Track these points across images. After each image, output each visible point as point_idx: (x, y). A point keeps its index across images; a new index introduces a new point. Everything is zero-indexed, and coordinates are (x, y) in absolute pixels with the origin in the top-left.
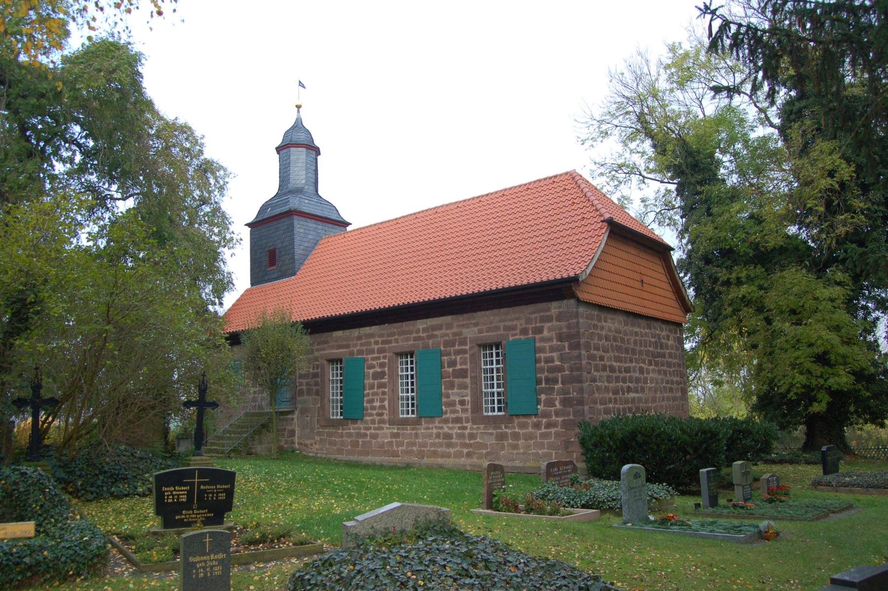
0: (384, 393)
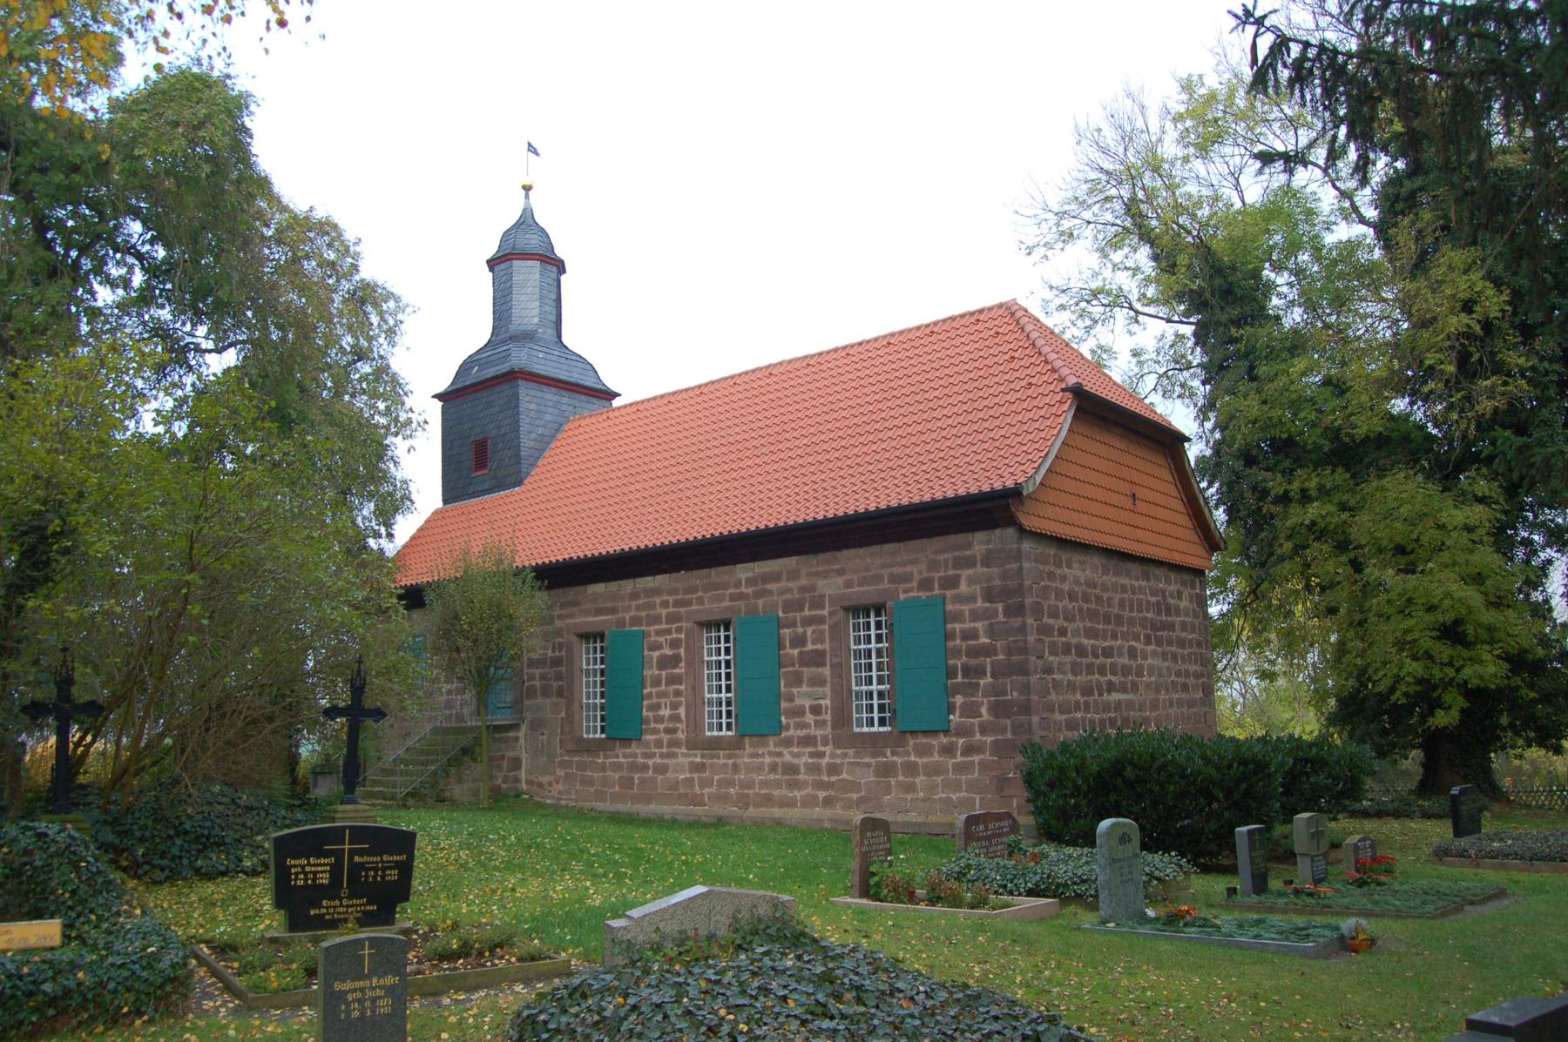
0: (678, 693)
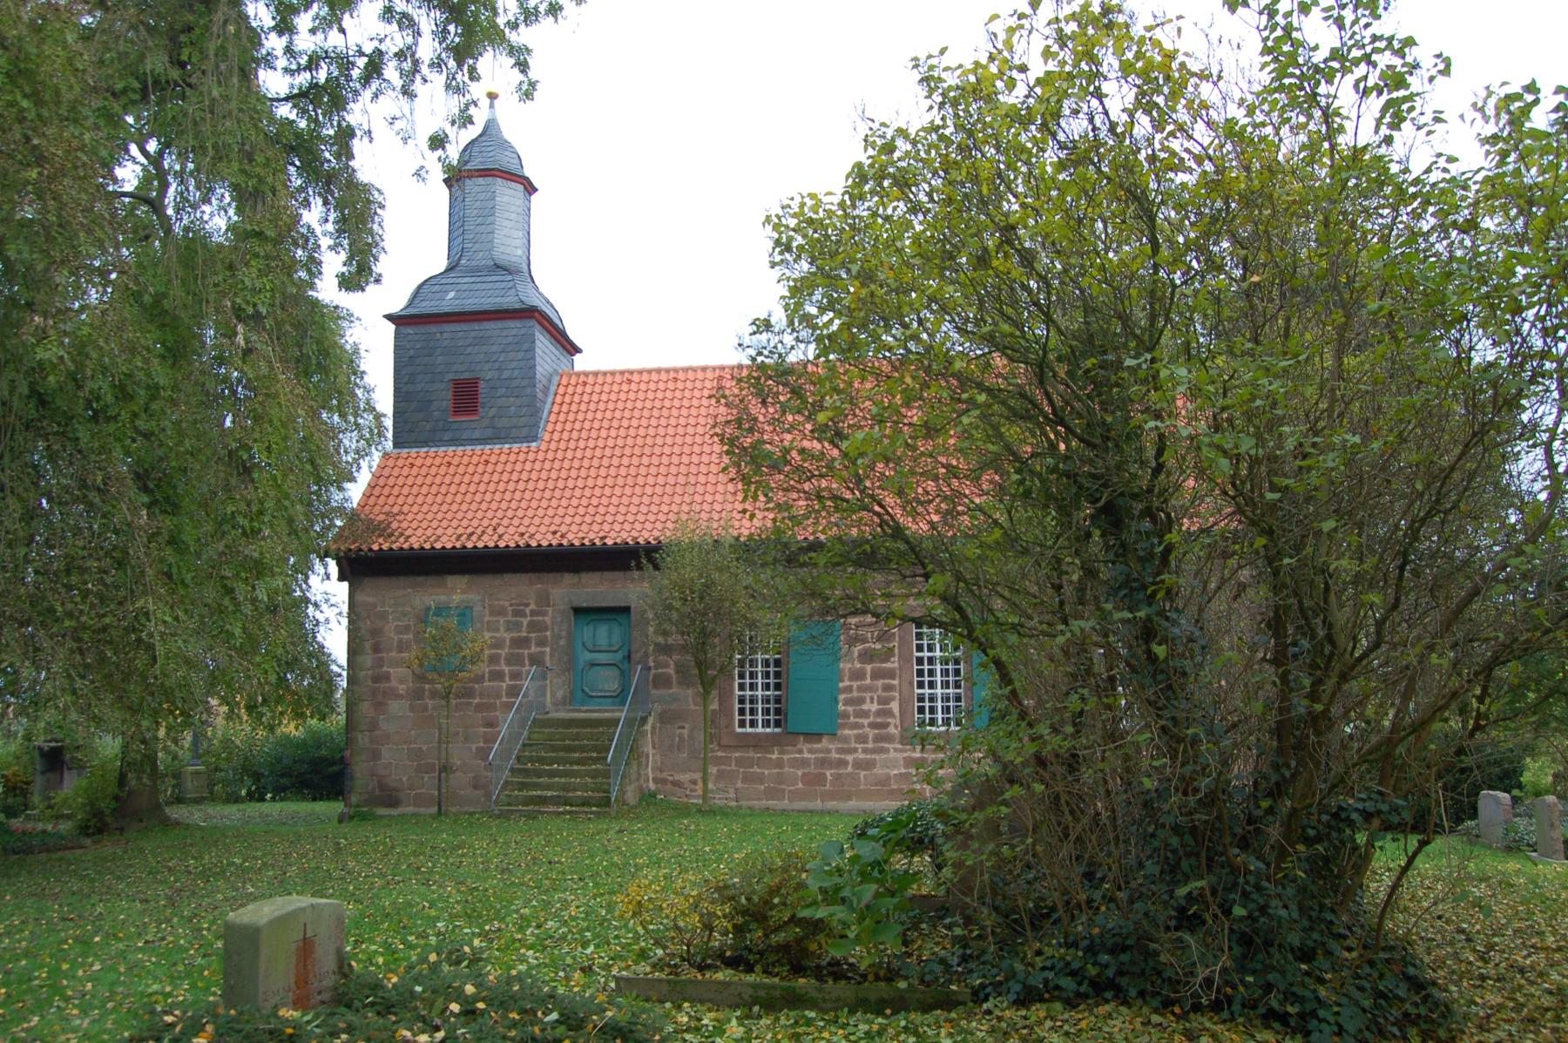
0: (888, 688)
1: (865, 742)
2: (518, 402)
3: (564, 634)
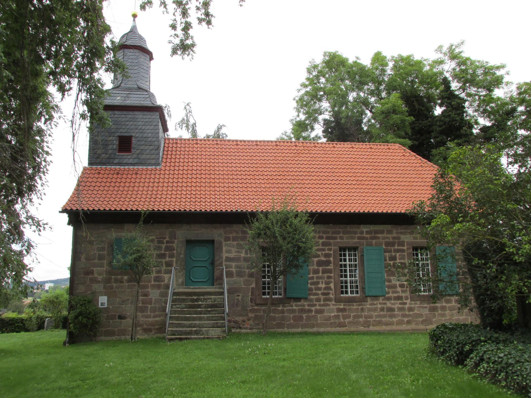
0: (329, 277)
1: (320, 301)
2: (151, 147)
3: (183, 252)
